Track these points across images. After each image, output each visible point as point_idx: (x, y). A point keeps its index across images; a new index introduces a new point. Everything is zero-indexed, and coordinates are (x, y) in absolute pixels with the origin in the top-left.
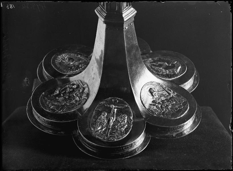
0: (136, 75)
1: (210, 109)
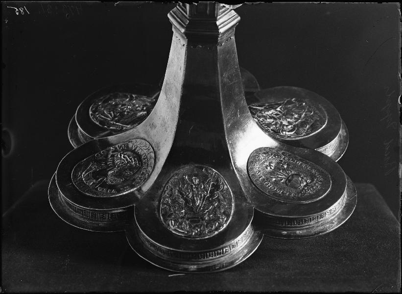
0: (237, 125)
1: (371, 188)
